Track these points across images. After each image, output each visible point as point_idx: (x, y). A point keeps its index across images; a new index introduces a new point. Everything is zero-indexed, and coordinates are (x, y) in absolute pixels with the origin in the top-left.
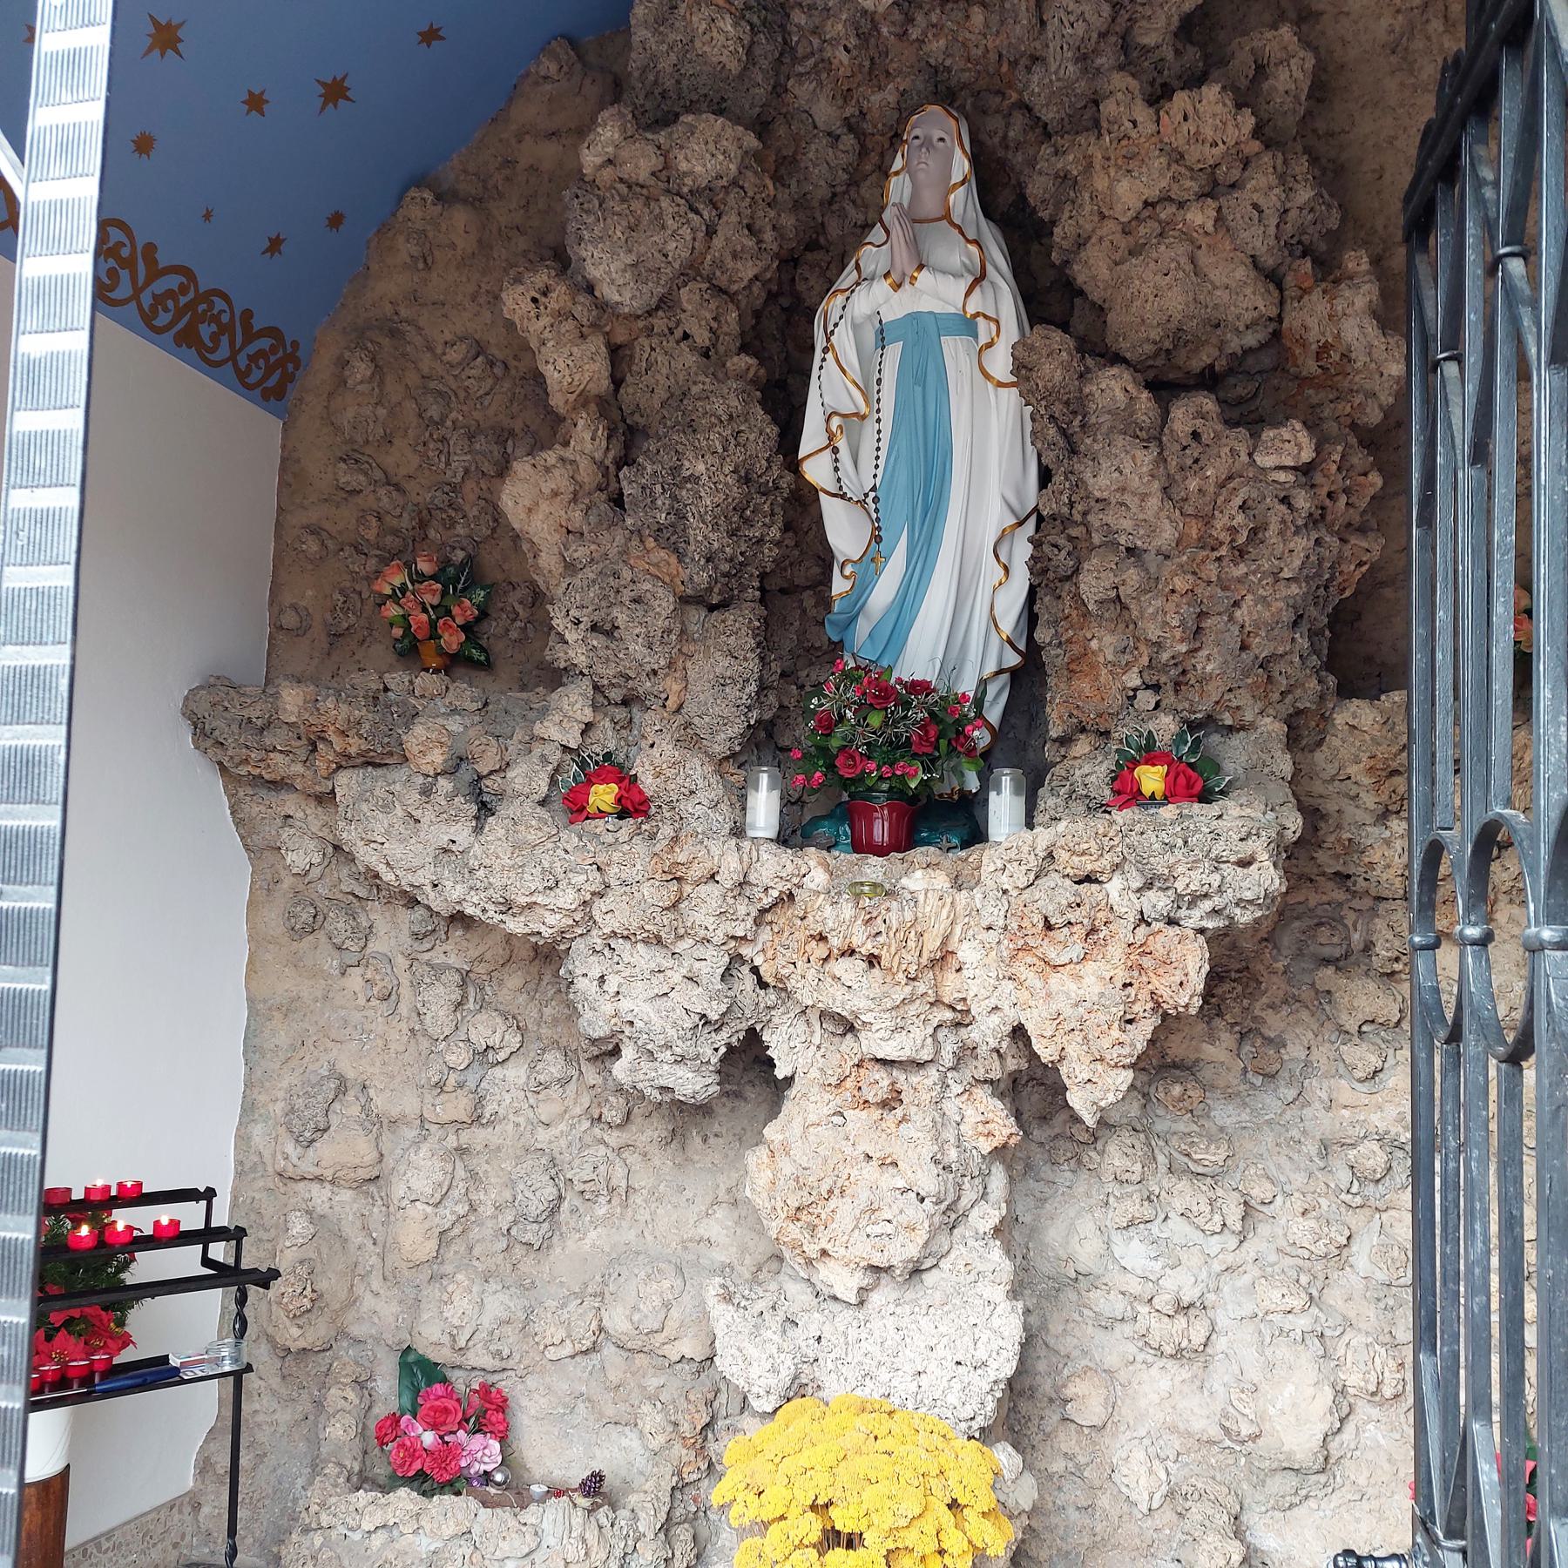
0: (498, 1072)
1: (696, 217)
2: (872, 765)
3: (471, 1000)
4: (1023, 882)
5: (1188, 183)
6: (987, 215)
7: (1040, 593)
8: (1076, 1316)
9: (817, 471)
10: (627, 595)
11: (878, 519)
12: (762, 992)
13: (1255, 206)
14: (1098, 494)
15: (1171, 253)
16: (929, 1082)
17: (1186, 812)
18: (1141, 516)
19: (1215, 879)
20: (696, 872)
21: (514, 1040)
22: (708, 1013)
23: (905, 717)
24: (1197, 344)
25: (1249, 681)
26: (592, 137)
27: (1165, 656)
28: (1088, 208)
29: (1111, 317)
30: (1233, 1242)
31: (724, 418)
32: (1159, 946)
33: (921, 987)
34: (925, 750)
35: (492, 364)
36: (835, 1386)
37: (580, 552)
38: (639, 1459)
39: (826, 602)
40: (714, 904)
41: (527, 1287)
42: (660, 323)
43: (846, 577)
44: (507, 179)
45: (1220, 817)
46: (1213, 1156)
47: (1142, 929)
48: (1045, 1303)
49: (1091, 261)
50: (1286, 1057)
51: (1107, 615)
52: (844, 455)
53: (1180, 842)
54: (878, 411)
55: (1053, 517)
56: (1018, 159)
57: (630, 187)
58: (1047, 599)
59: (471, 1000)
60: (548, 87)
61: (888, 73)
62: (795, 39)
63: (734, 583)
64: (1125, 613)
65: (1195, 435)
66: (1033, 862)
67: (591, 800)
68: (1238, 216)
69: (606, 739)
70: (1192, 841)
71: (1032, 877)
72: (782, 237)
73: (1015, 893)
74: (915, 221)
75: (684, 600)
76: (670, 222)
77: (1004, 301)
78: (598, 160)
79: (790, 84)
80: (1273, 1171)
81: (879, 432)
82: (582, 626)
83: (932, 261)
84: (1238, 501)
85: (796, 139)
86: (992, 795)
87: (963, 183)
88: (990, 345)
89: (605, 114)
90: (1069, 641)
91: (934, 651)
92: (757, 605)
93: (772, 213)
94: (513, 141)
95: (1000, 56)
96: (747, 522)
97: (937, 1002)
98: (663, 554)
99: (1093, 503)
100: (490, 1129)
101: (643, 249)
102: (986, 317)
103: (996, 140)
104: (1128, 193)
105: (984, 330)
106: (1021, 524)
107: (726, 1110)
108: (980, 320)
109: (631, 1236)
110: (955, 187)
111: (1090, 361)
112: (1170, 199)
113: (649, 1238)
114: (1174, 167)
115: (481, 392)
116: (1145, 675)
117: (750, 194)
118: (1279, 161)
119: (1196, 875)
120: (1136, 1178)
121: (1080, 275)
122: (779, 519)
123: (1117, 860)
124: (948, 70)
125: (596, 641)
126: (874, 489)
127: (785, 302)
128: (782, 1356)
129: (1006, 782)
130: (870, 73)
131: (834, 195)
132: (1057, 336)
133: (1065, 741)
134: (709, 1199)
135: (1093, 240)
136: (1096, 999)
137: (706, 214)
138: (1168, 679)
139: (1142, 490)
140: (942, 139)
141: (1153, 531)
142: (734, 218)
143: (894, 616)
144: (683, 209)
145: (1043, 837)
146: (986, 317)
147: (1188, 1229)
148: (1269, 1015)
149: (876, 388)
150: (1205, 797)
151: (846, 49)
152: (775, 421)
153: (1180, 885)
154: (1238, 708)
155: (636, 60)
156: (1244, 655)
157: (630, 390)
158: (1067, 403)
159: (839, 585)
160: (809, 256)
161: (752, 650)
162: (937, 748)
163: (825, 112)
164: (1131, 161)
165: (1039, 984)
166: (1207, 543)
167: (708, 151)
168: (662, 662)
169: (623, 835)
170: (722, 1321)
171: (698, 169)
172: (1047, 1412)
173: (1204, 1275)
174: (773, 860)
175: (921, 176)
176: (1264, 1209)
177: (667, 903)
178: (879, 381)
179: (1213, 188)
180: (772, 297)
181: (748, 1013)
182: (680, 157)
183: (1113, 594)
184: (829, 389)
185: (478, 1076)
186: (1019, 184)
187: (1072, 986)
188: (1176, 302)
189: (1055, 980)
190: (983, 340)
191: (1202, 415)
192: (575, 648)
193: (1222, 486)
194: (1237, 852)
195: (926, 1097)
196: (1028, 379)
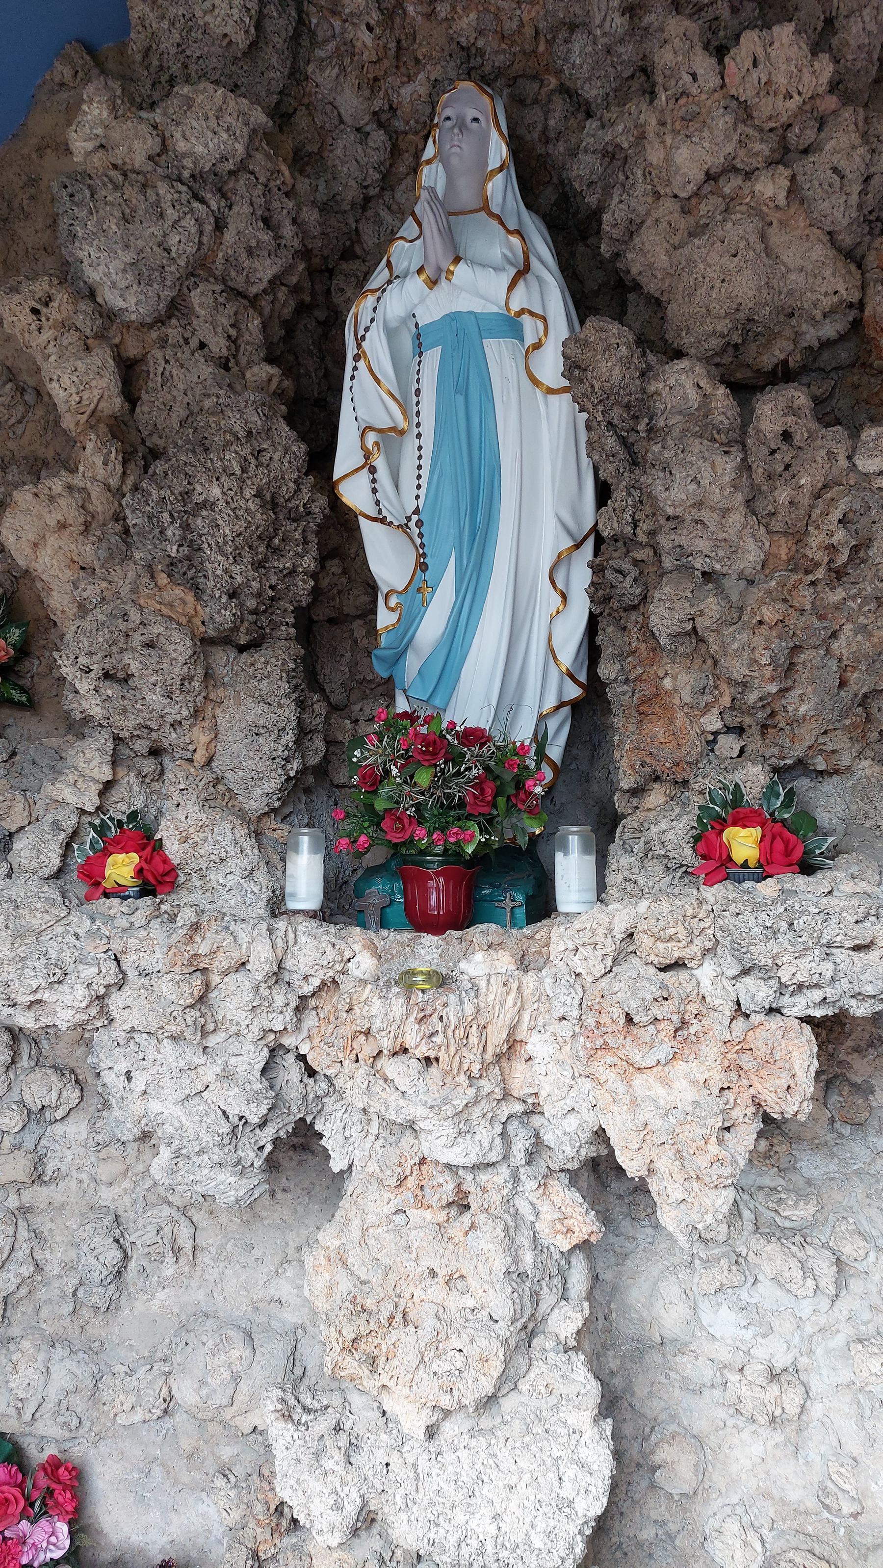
0: (58, 1129)
1: (200, 206)
2: (420, 832)
3: (25, 1057)
4: (599, 970)
5: (757, 147)
6: (528, 206)
7: (603, 623)
8: (663, 1379)
9: (355, 494)
10: (137, 639)
11: (422, 545)
12: (311, 1081)
13: (835, 170)
14: (670, 511)
15: (739, 230)
16: (499, 1180)
17: (788, 886)
18: (721, 535)
19: (827, 969)
20: (221, 962)
21: (72, 1095)
22: (247, 1115)
23: (458, 774)
24: (771, 336)
25: (847, 722)
26: (79, 119)
27: (752, 698)
28: (640, 188)
29: (673, 310)
30: (825, 1303)
31: (242, 434)
32: (760, 1043)
33: (486, 1086)
34: (482, 810)
35: (22, 391)
36: (405, 1527)
37: (90, 591)
38: (216, 1526)
39: (372, 631)
40: (246, 996)
41: (94, 1351)
42: (173, 332)
43: (392, 609)
44: (32, 198)
45: (830, 892)
46: (799, 1213)
47: (740, 1024)
48: (629, 1365)
49: (648, 247)
50: (875, 1104)
51: (681, 650)
52: (383, 474)
53: (784, 926)
54: (418, 425)
55: (615, 539)
57: (125, 175)
58: (610, 629)
59: (25, 1057)
60: (64, 95)
61: (417, 61)
62: (314, 21)
63: (264, 620)
64: (702, 646)
65: (786, 436)
66: (610, 948)
67: (107, 873)
68: (816, 183)
69: (129, 797)
70: (799, 924)
71: (609, 963)
73: (590, 979)
74: (451, 214)
75: (206, 643)
76: (170, 211)
77: (550, 295)
78: (90, 146)
79: (310, 69)
80: (865, 1226)
81: (420, 448)
82: (92, 675)
83: (470, 254)
84: (837, 514)
86: (559, 857)
87: (501, 169)
88: (537, 346)
89: (91, 88)
90: (638, 679)
91: (488, 698)
93: (290, 204)
94: (34, 156)
95: (537, 33)
96: (277, 551)
97: (507, 1095)
98: (178, 591)
99: (663, 522)
100: (53, 1187)
101: (141, 243)
102: (532, 314)
103: (536, 135)
104: (688, 161)
105: (530, 328)
106: (578, 546)
107: (294, 1164)
108: (526, 318)
109: (201, 1295)
110: (493, 173)
111: (651, 358)
112: (735, 170)
113: (218, 1298)
114: (741, 127)
115: (13, 420)
116: (727, 717)
117: (262, 179)
118: (861, 118)
119: (804, 964)
120: (721, 1238)
122: (313, 547)
123: (709, 945)
124: (481, 53)
125: (110, 690)
126: (417, 511)
128: (346, 1489)
129: (574, 841)
130: (397, 57)
131: (367, 199)
132: (614, 328)
133: (637, 792)
134: (278, 1259)
135: (648, 223)
136: (689, 1108)
137: (214, 204)
138: (756, 721)
139: (724, 504)
140: (476, 120)
141: (734, 551)
142: (246, 209)
143: (444, 652)
144: (185, 197)
145: (621, 915)
146: (532, 314)
147: (779, 1293)
148: (856, 1061)
149: (415, 399)
150: (808, 868)
151: (370, 28)
152: (302, 437)
153: (785, 975)
154: (834, 752)
155: (137, 40)
156: (843, 694)
157: (146, 409)
158: (628, 407)
159: (385, 618)
160: (344, 266)
162: (495, 806)
163: (351, 103)
164: (692, 122)
165: (621, 1088)
166: (800, 565)
167: (210, 129)
168: (185, 713)
169: (139, 919)
170: (281, 1442)
171: (200, 149)
172: (635, 1477)
173: (796, 1340)
174: (312, 943)
175: (455, 161)
176: (856, 1265)
177: (190, 1001)
178: (418, 392)
179: (784, 154)
180: (302, 309)
181: (294, 1109)
182: (178, 135)
183: (689, 626)
184: (363, 403)
185: (36, 1135)
186: (562, 182)
187: (659, 1091)
188: (746, 288)
189: (639, 1081)
190: (529, 340)
191: (791, 410)
192: (88, 698)
193: (817, 496)
194: (853, 938)
195: (496, 1198)
196: (581, 381)
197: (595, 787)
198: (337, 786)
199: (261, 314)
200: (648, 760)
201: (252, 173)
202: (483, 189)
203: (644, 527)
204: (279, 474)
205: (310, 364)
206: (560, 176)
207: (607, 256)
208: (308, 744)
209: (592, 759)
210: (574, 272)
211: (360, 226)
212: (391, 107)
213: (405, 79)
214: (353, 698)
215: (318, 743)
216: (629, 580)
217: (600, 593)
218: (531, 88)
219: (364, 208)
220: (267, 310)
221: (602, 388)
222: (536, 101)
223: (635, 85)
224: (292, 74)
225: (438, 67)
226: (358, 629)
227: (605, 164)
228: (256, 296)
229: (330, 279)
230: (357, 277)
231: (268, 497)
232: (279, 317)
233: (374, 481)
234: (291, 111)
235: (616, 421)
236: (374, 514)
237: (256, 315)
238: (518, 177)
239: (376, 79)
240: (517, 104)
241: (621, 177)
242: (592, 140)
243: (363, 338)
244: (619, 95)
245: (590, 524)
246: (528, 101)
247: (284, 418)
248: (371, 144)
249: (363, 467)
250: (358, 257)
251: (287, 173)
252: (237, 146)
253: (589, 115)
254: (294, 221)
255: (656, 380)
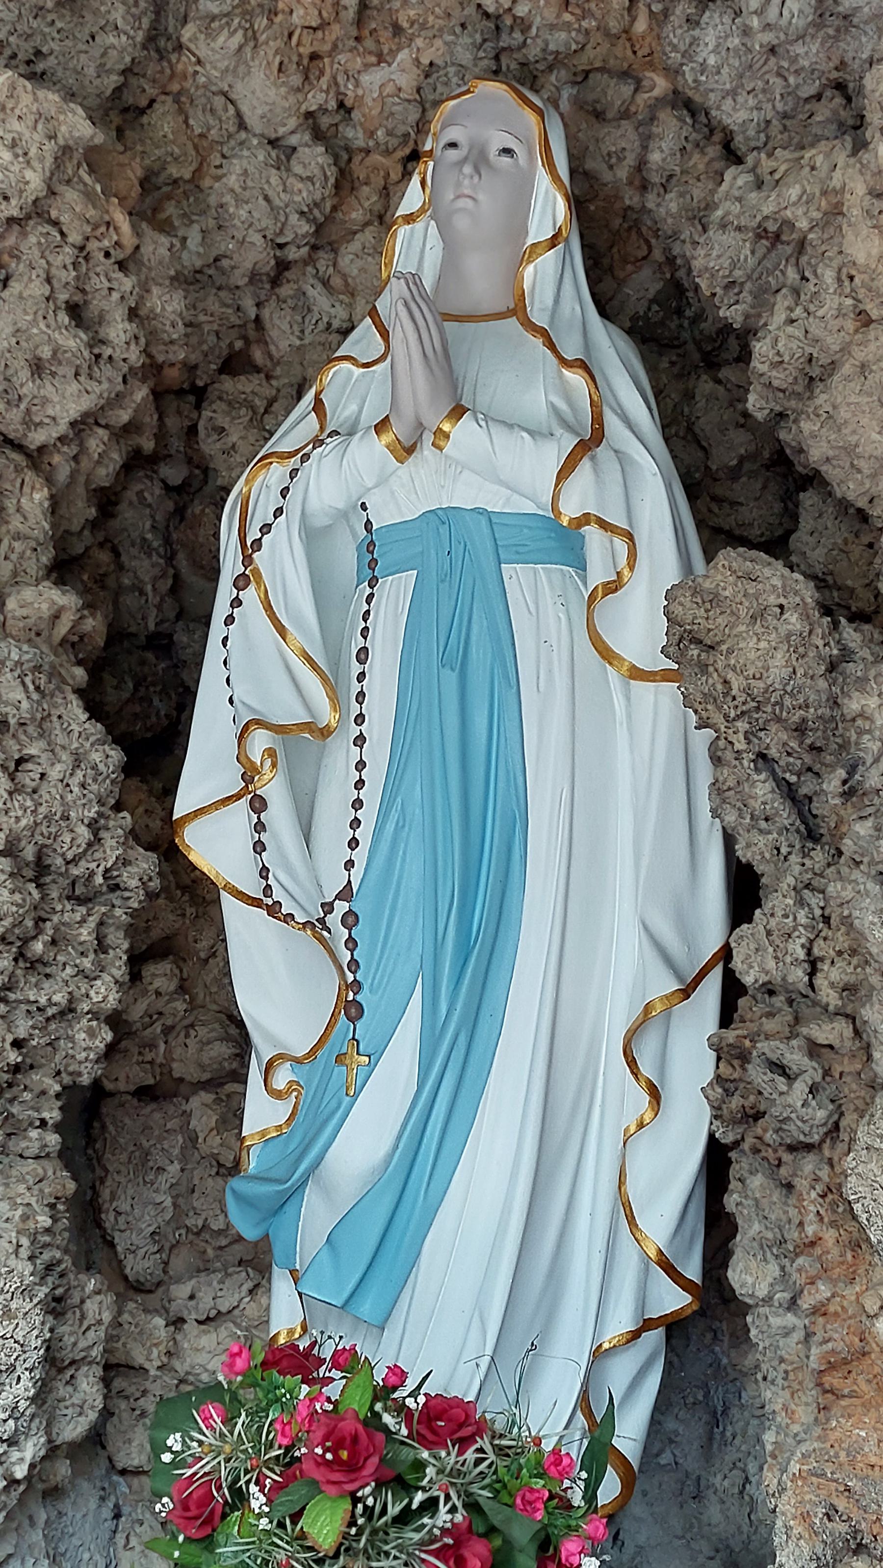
6: (603, 312)
7: (740, 1165)
9: (216, 847)
11: (354, 965)
23: (405, 1518)
28: (831, 303)
43: (278, 1095)
49: (844, 414)
54: (360, 719)
56: (668, 207)
61: (397, 30)
72: (152, 336)
74: (448, 317)
77: (644, 490)
79: (187, 33)
81: (361, 765)
83: (483, 400)
85: (202, 146)
87: (553, 242)
88: (613, 587)
90: (820, 1310)
91: (480, 1310)
92: (50, 1168)
93: (127, 283)
102: (603, 525)
103: (622, 173)
106: (686, 993)
108: (592, 532)
121: (815, 441)
126: (346, 894)
127: (174, 473)
130: (359, 22)
131: (283, 266)
132: (773, 574)
135: (847, 369)
140: (507, 151)
142: (38, 289)
146: (603, 525)
158: (800, 729)
159: (261, 1112)
160: (228, 384)
161: (26, 1291)
163: (263, 95)
175: (461, 223)
178: (363, 655)
180: (136, 463)
184: (245, 671)
186: (671, 261)
196: (704, 668)
197: (714, 1512)
198: (123, 1472)
199: (49, 481)
200: (841, 1504)
201: (56, 223)
202: (516, 277)
203: (832, 974)
204: (57, 808)
205: (144, 567)
206: (667, 250)
207: (760, 416)
208: (63, 1391)
209: (711, 1444)
210: (689, 429)
211: (266, 313)
212: (341, 105)
213: (373, 59)
214: (178, 1264)
215: (88, 1387)
216: (800, 1088)
217: (736, 1102)
218: (618, 93)
219: (275, 282)
220: (63, 474)
221: (747, 691)
222: (625, 115)
223: (823, 112)
224: (151, 39)
225: (438, 43)
226: (201, 1112)
227: (760, 253)
228: (42, 449)
229: (198, 407)
230: (253, 409)
231: (29, 853)
232: (87, 482)
233: (260, 827)
234: (144, 103)
235: (773, 753)
236: (254, 890)
237: (39, 482)
238: (585, 247)
239: (314, 57)
240: (589, 115)
241: (792, 275)
242: (736, 208)
243: (257, 544)
244: (793, 128)
245: (712, 944)
246: (610, 115)
247: (78, 691)
248: (298, 169)
249: (238, 797)
250: (258, 370)
251: (125, 226)
252: (29, 175)
253: (732, 156)
254: (133, 314)
255: (862, 691)
